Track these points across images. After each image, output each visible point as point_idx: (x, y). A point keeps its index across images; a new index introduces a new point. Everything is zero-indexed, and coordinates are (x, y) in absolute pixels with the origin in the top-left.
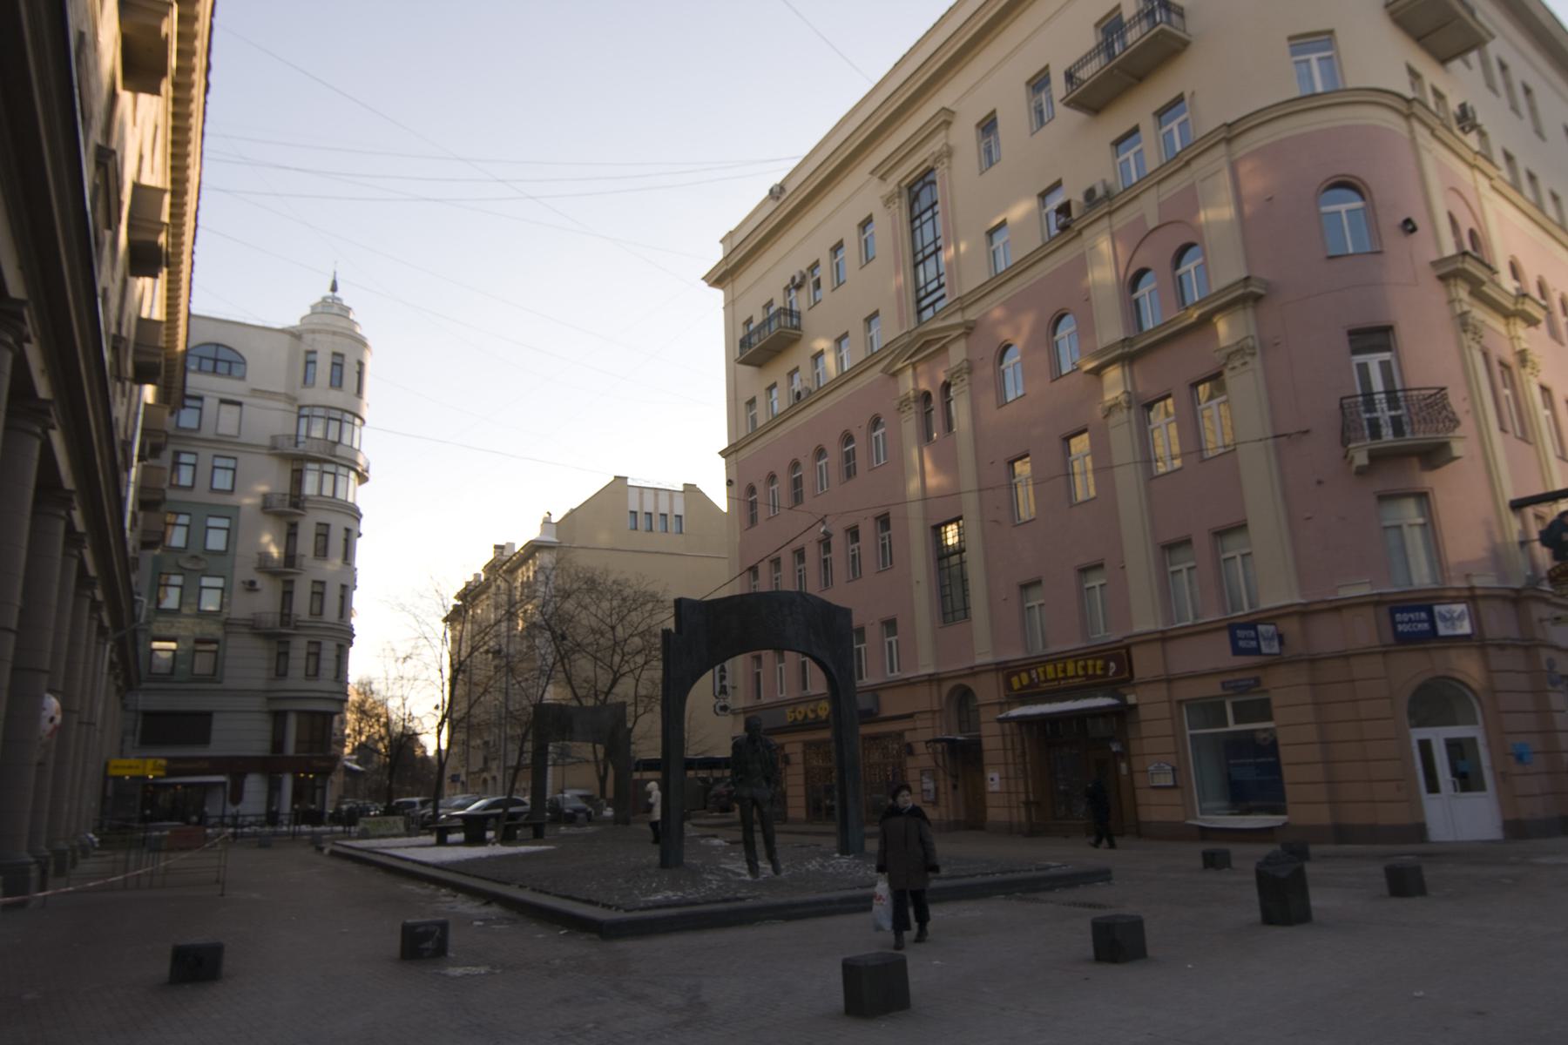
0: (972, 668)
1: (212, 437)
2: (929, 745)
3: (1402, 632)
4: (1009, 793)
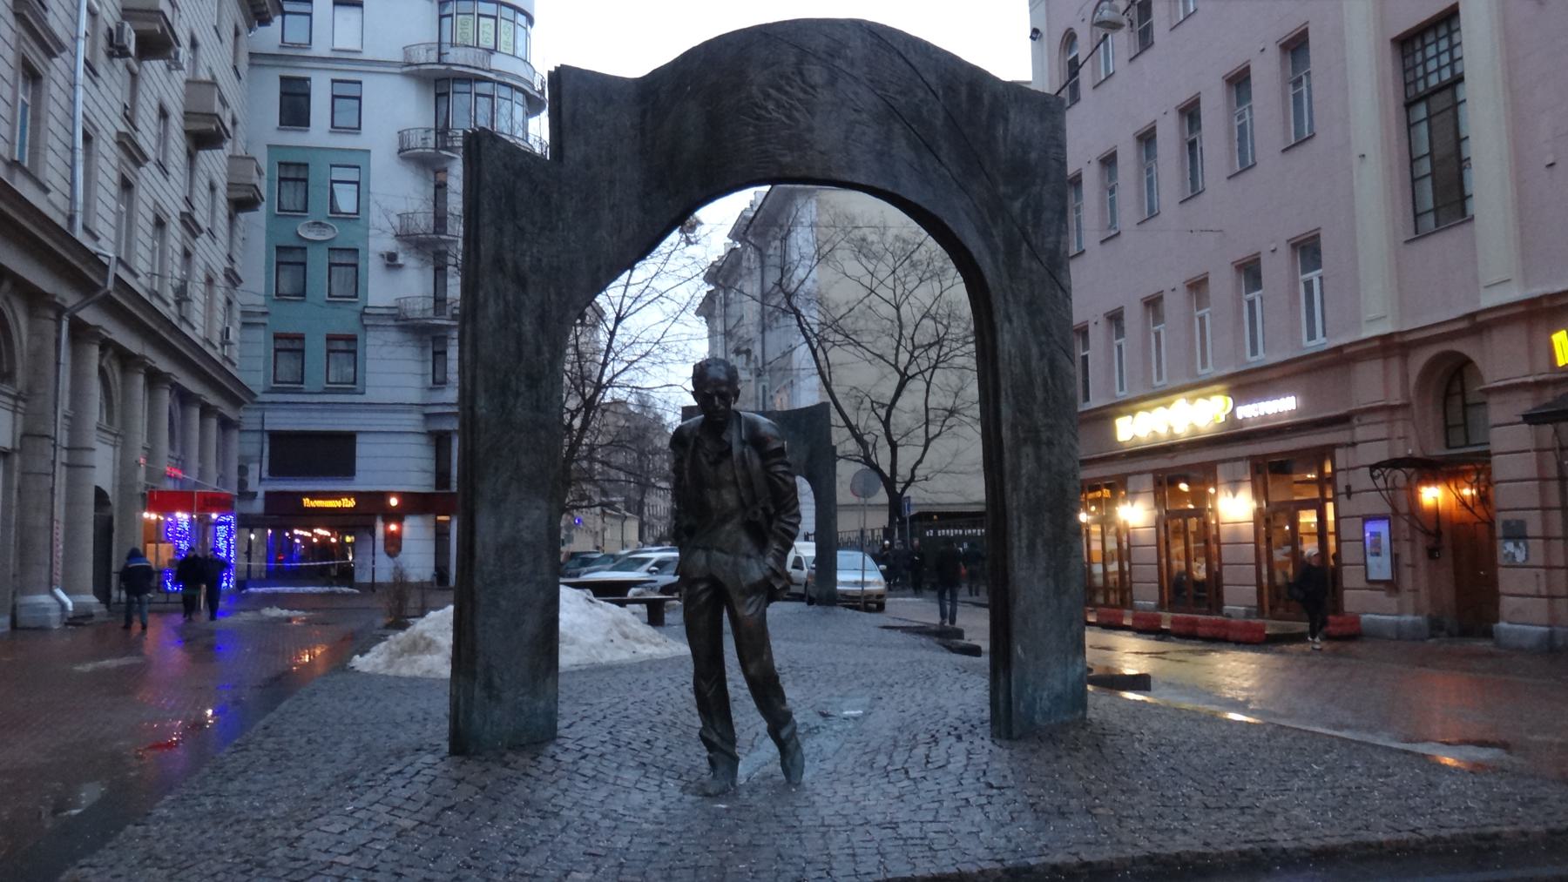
0: (1472, 316)
1: (327, 53)
2: (1377, 472)
3: (1436, 514)
4: (1549, 567)
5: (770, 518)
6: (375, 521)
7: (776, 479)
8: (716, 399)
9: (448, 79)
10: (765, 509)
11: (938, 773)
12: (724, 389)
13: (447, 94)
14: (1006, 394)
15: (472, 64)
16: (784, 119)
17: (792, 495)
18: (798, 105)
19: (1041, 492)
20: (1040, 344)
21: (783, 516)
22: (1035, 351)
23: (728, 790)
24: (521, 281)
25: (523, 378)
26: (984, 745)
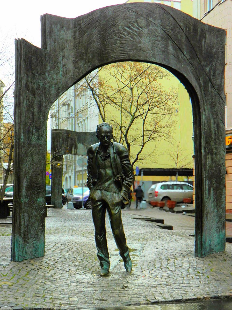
5: (123, 179)
8: (106, 137)
10: (122, 177)
11: (180, 269)
12: (109, 134)
14: (203, 137)
16: (130, 38)
19: (213, 171)
20: (214, 119)
22: (212, 121)
23: (107, 274)
24: (33, 93)
25: (34, 128)
26: (194, 260)
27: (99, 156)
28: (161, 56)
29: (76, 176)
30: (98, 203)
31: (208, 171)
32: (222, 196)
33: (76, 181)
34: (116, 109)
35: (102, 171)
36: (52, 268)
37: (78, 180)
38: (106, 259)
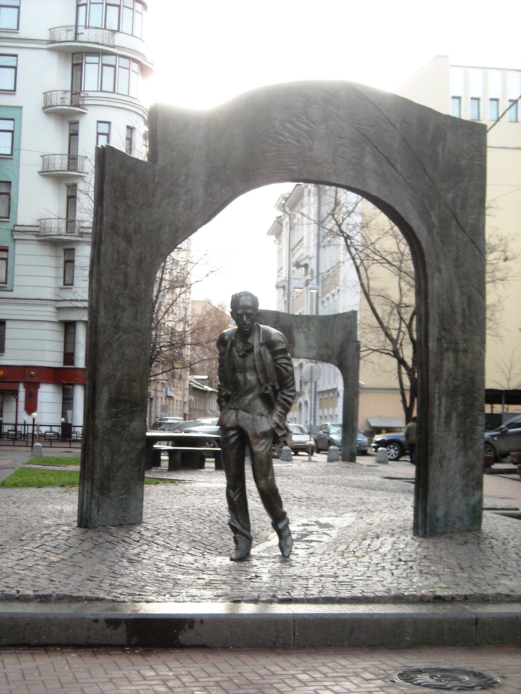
5: (276, 392)
6: (18, 387)
7: (281, 368)
8: (244, 316)
9: (82, 53)
10: (273, 387)
12: (249, 311)
13: (81, 65)
14: (434, 319)
15: (101, 42)
16: (294, 142)
17: (291, 378)
18: (304, 134)
19: (458, 383)
20: (462, 287)
21: (285, 391)
24: (128, 240)
26: (409, 537)
27: (234, 350)
28: (350, 173)
29: (318, 402)
30: (229, 433)
31: (447, 382)
32: (476, 429)
33: (318, 410)
34: (392, 273)
35: (240, 377)
36: (145, 542)
37: (320, 408)
38: (245, 531)
